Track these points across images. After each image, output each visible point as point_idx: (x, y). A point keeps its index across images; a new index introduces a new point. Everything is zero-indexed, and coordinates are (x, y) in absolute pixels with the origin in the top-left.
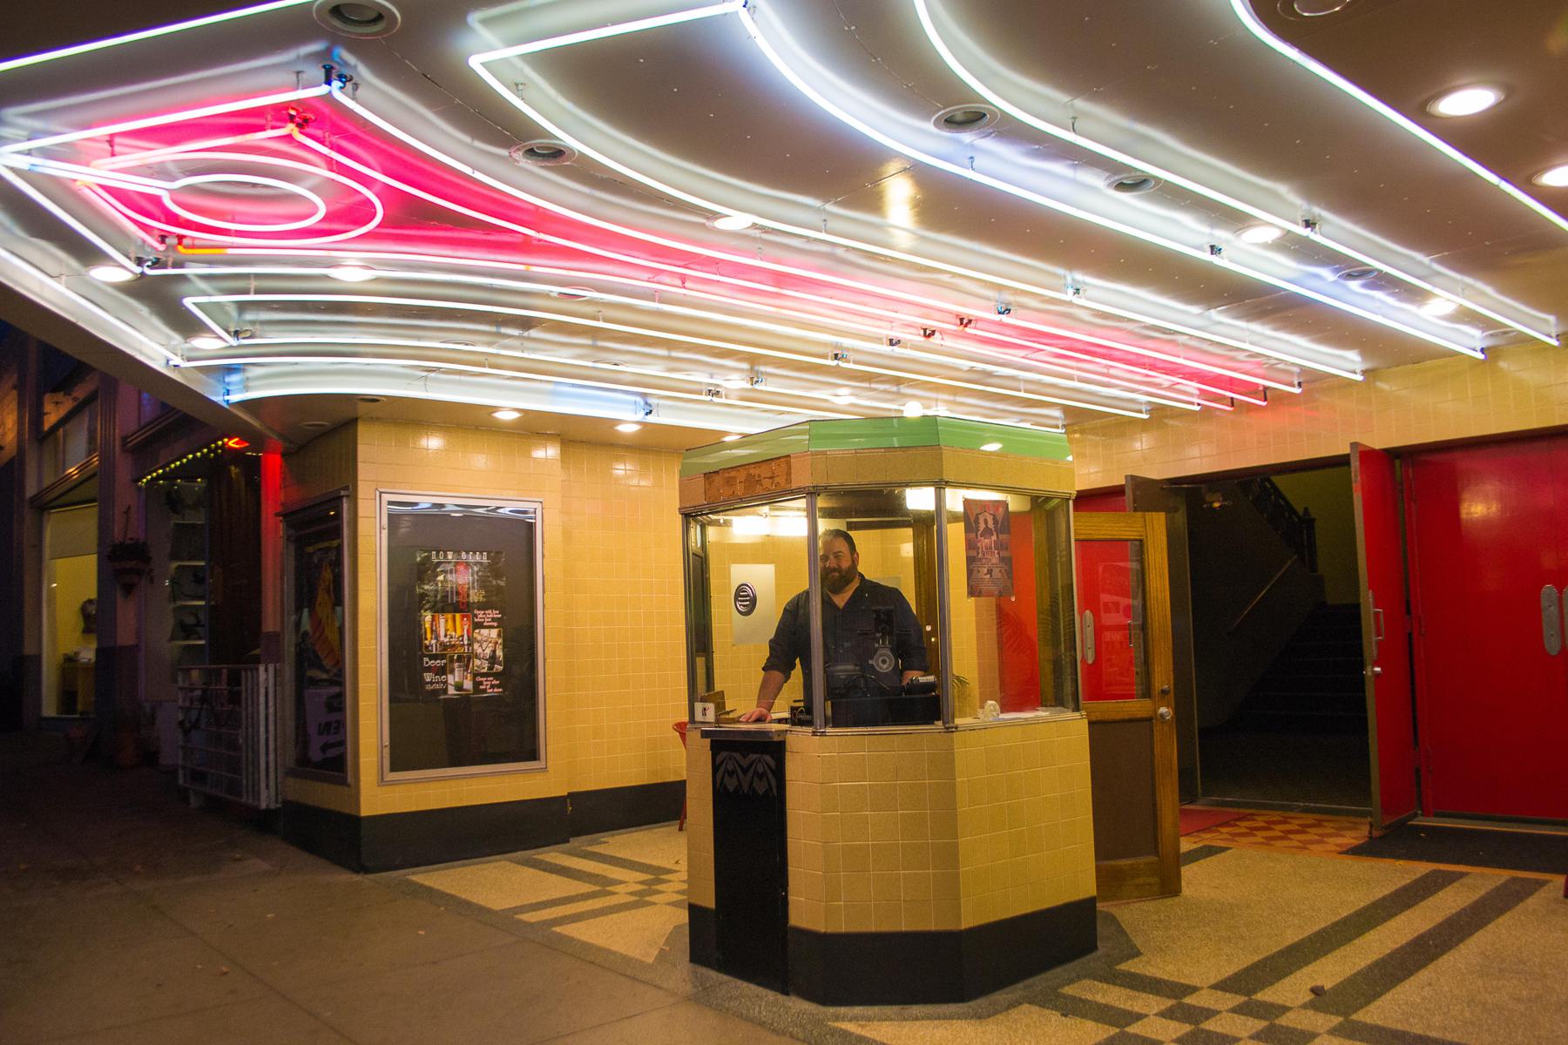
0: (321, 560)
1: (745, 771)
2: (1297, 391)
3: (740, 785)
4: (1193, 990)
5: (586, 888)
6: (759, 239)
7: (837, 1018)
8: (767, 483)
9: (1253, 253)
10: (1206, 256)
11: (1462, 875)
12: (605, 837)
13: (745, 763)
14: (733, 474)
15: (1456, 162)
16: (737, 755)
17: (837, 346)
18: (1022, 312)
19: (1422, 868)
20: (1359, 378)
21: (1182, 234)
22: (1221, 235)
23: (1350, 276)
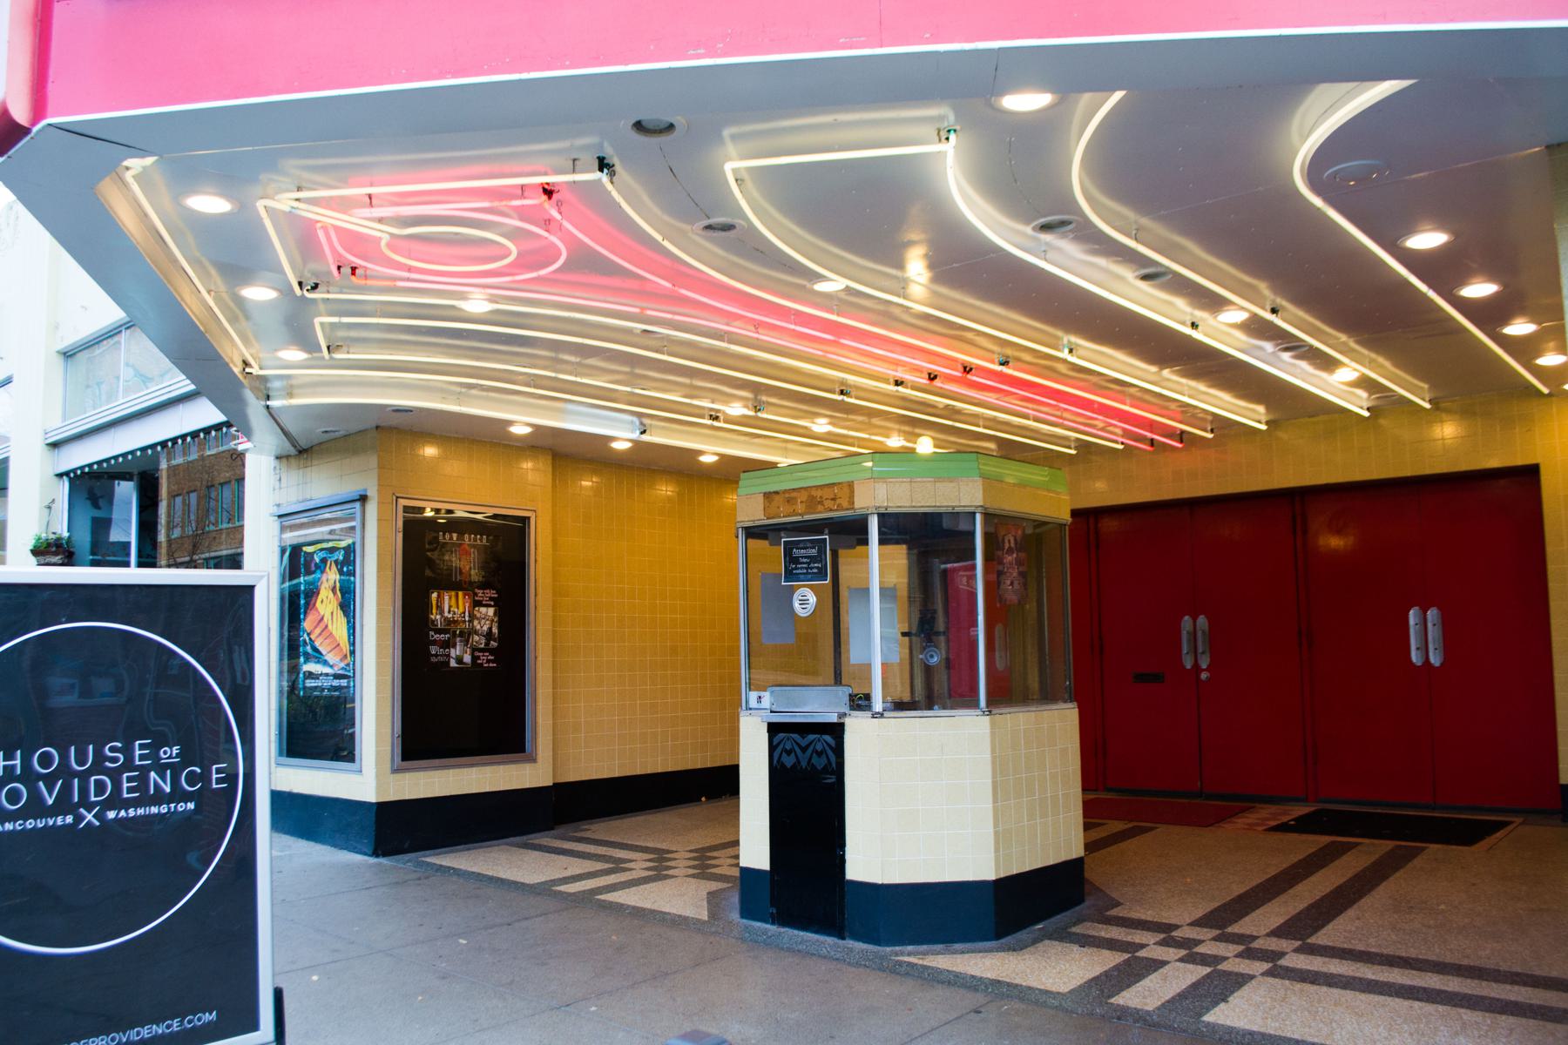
0: (324, 561)
1: (804, 750)
2: (1210, 436)
3: (798, 761)
4: (1177, 927)
5: (599, 866)
6: (849, 301)
7: (902, 954)
8: (829, 504)
9: (1222, 330)
10: (1188, 331)
11: (1357, 844)
12: (595, 827)
13: (804, 743)
14: (794, 494)
15: (1399, 275)
16: (795, 736)
17: (843, 382)
18: (1020, 365)
19: (1325, 839)
20: (1263, 427)
21: (1169, 312)
22: (1200, 315)
23: (1286, 349)
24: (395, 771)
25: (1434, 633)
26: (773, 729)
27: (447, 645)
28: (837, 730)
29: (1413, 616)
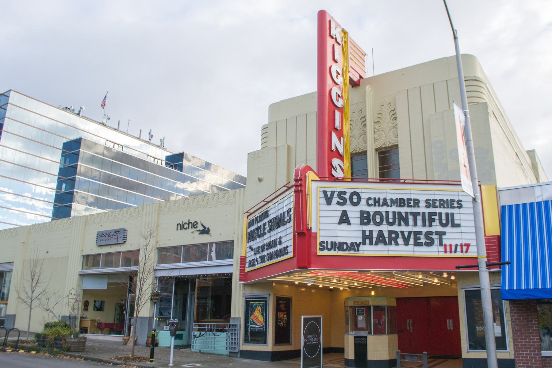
24: (275, 345)
25: (451, 324)
26: (355, 337)
27: (280, 322)
28: (366, 337)
29: (448, 320)
